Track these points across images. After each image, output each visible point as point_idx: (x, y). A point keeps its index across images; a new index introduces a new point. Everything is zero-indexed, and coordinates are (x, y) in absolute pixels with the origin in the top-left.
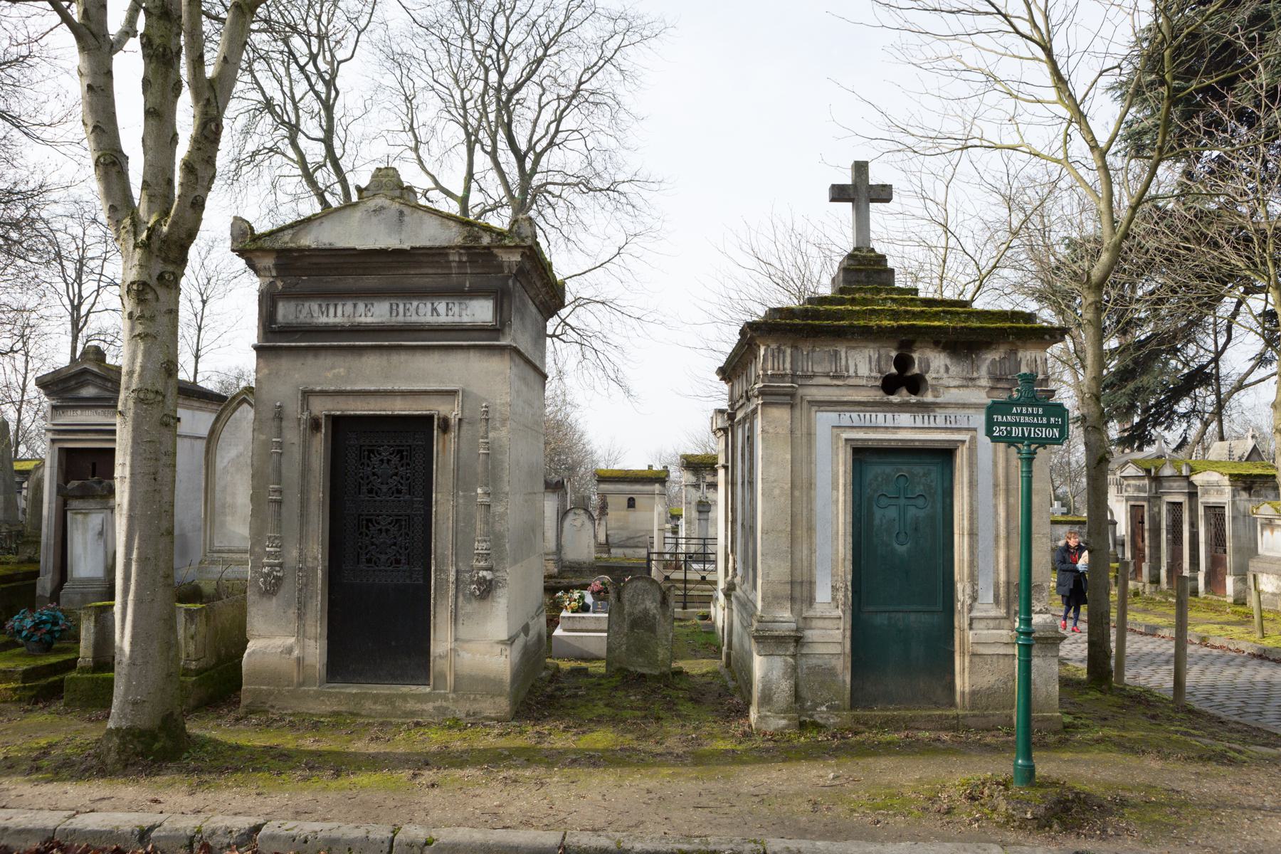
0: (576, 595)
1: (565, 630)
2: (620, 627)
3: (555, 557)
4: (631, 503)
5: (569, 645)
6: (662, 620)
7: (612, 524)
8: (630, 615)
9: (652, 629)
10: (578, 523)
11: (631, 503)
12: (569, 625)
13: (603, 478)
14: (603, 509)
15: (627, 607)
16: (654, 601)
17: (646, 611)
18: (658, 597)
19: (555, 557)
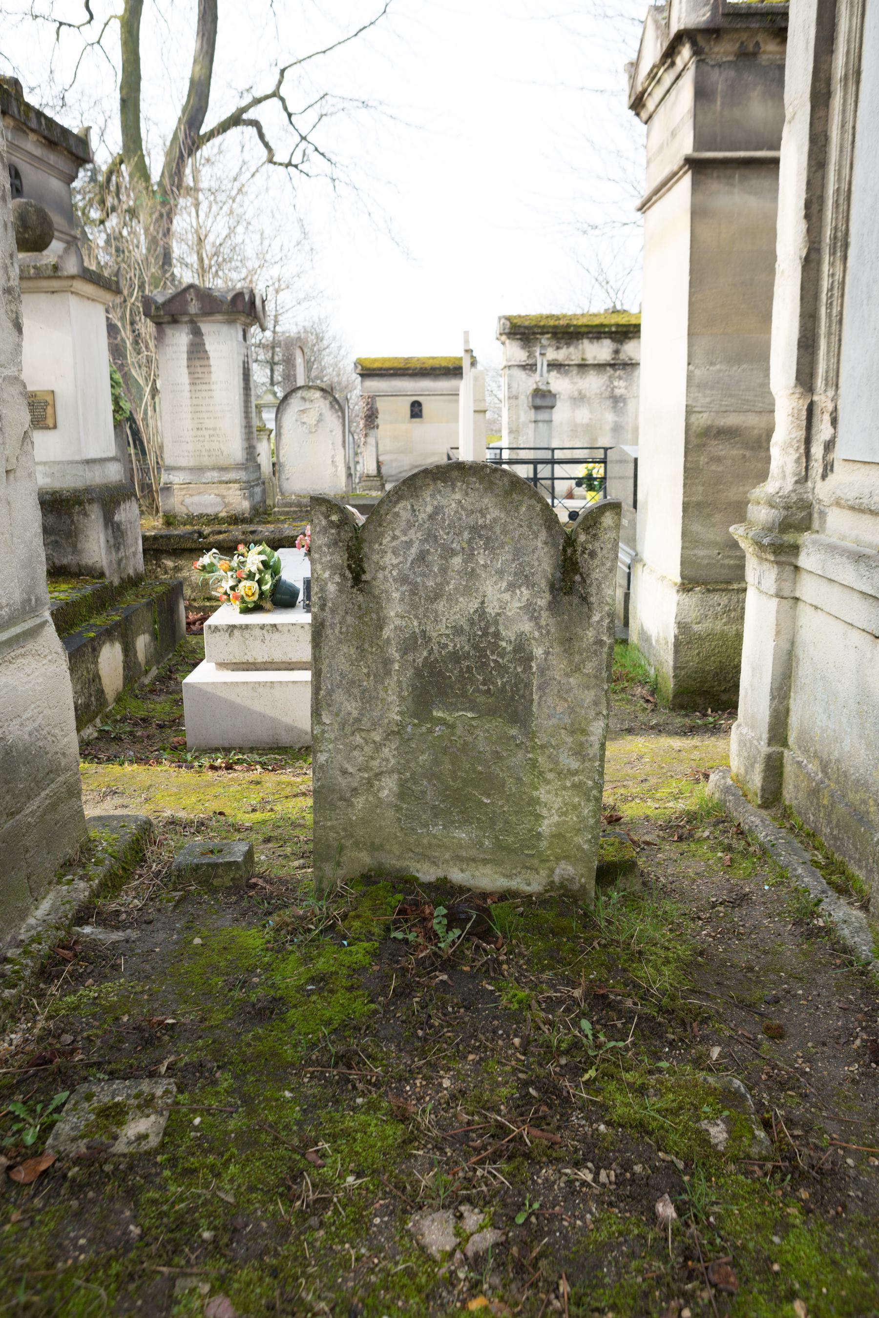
0: (254, 558)
1: (223, 665)
2: (367, 699)
3: (242, 475)
4: (416, 410)
5: (234, 708)
6: (559, 666)
7: (386, 445)
8: (410, 645)
9: (512, 706)
10: (311, 418)
11: (416, 410)
12: (234, 649)
13: (368, 372)
14: (371, 417)
15: (395, 611)
16: (523, 578)
17: (484, 628)
18: (543, 561)
19: (242, 475)
